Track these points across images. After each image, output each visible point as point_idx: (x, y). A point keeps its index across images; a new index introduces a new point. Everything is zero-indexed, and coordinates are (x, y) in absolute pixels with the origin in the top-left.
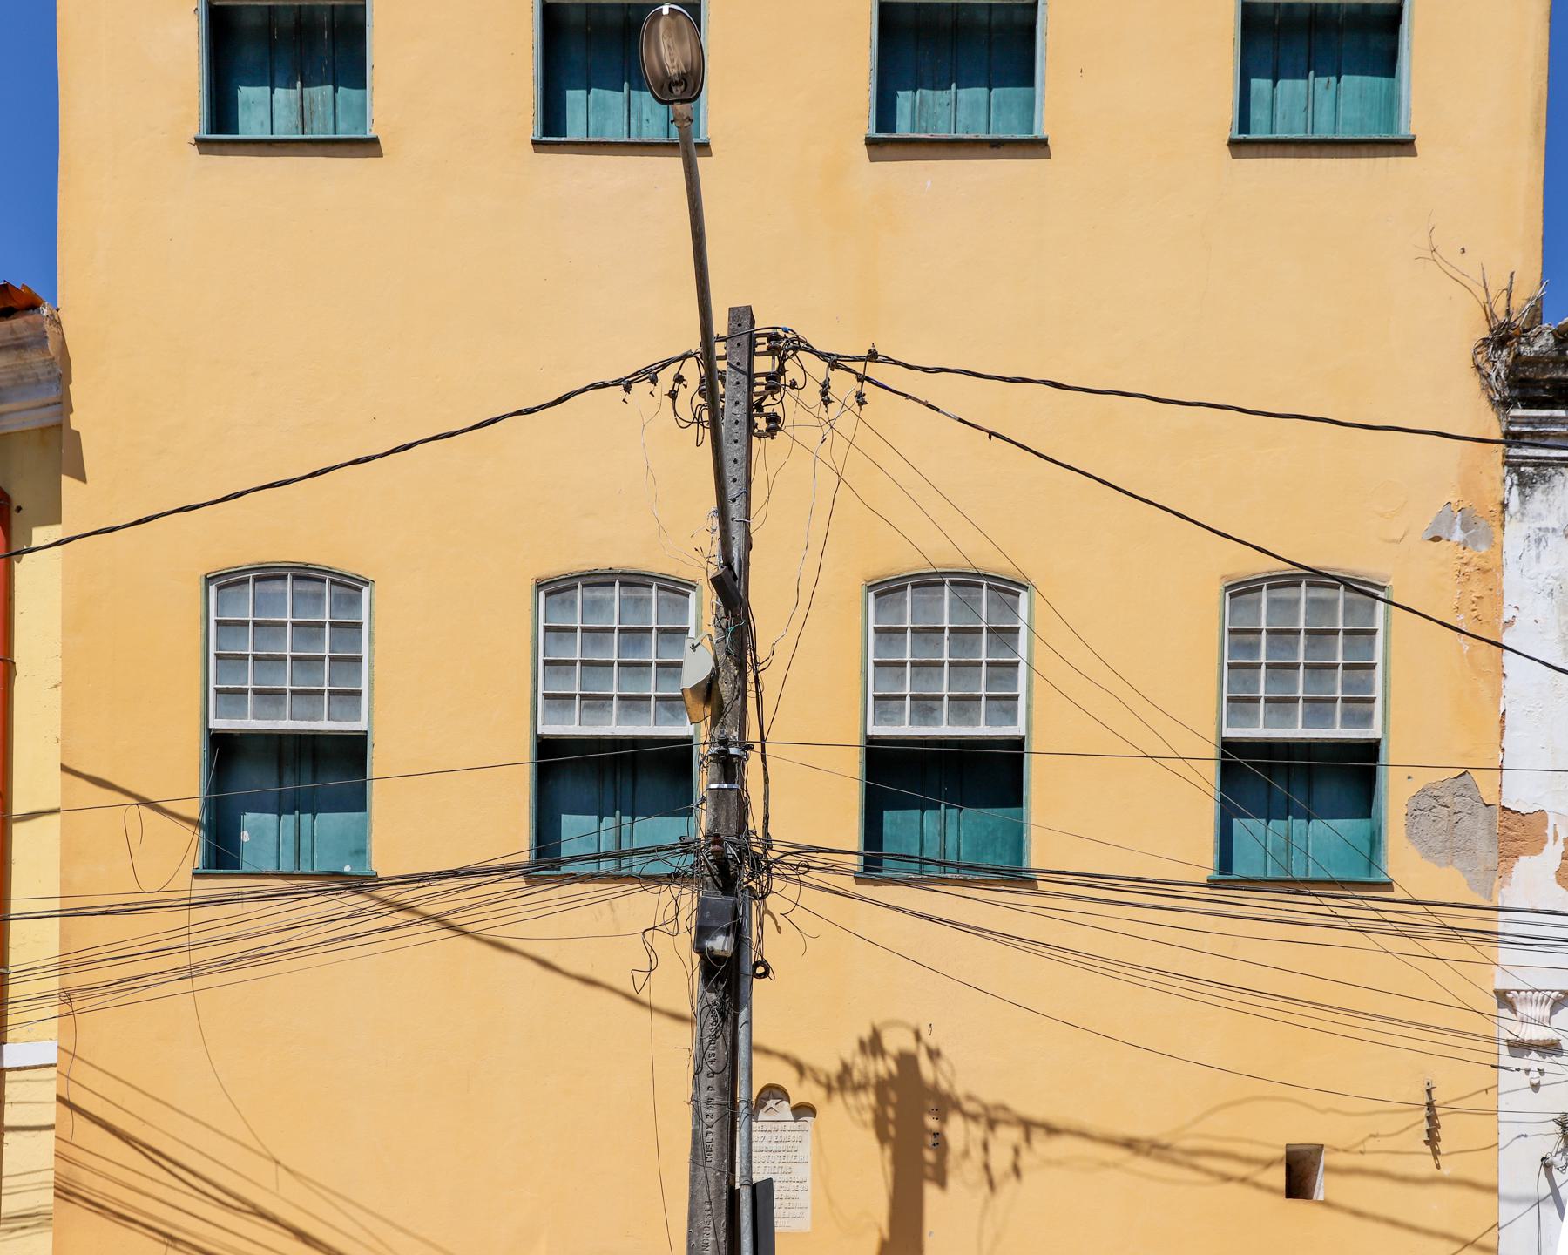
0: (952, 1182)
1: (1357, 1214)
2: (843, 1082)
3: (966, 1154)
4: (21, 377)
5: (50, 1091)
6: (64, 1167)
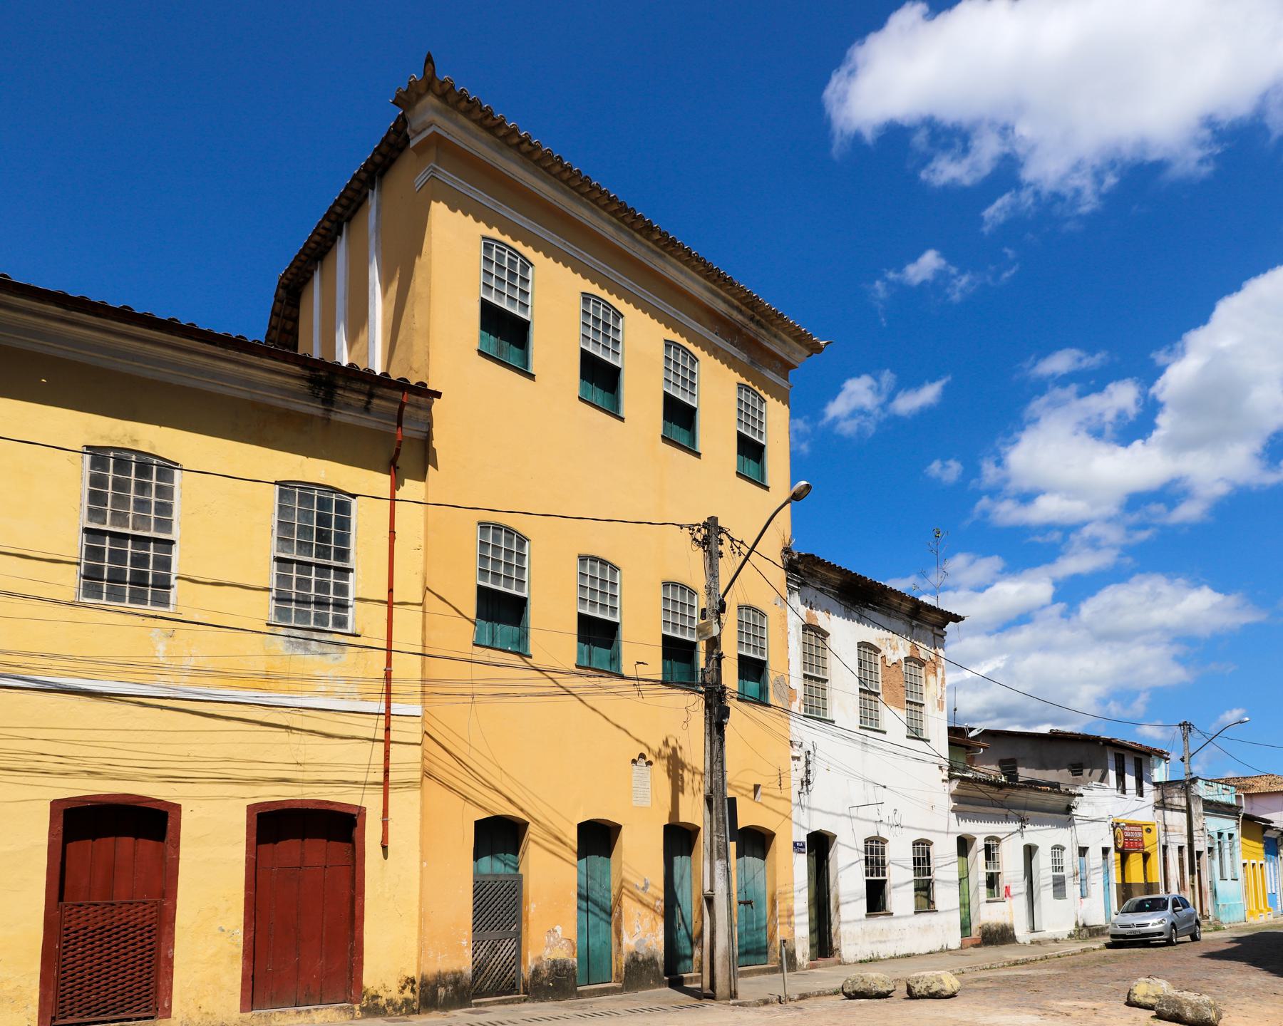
2: (659, 755)
5: (418, 729)
6: (426, 762)
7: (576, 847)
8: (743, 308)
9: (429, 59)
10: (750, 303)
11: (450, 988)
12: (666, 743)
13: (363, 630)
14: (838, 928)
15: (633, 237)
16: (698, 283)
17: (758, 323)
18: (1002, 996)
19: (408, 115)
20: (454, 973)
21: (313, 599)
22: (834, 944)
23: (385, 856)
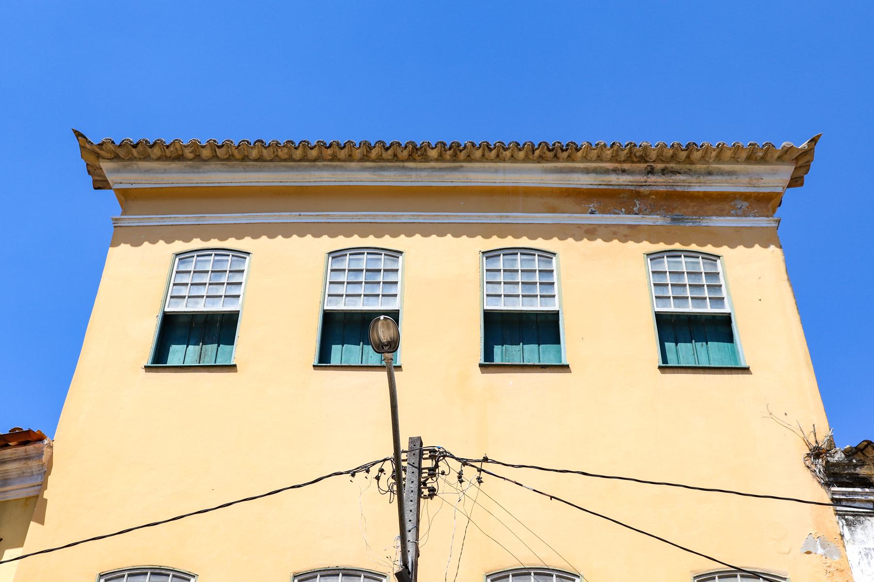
4: (24, 473)
8: (626, 166)
9: (78, 134)
10: (636, 156)
15: (404, 168)
16: (530, 171)
17: (664, 172)
18: (213, 166)
19: (111, 193)
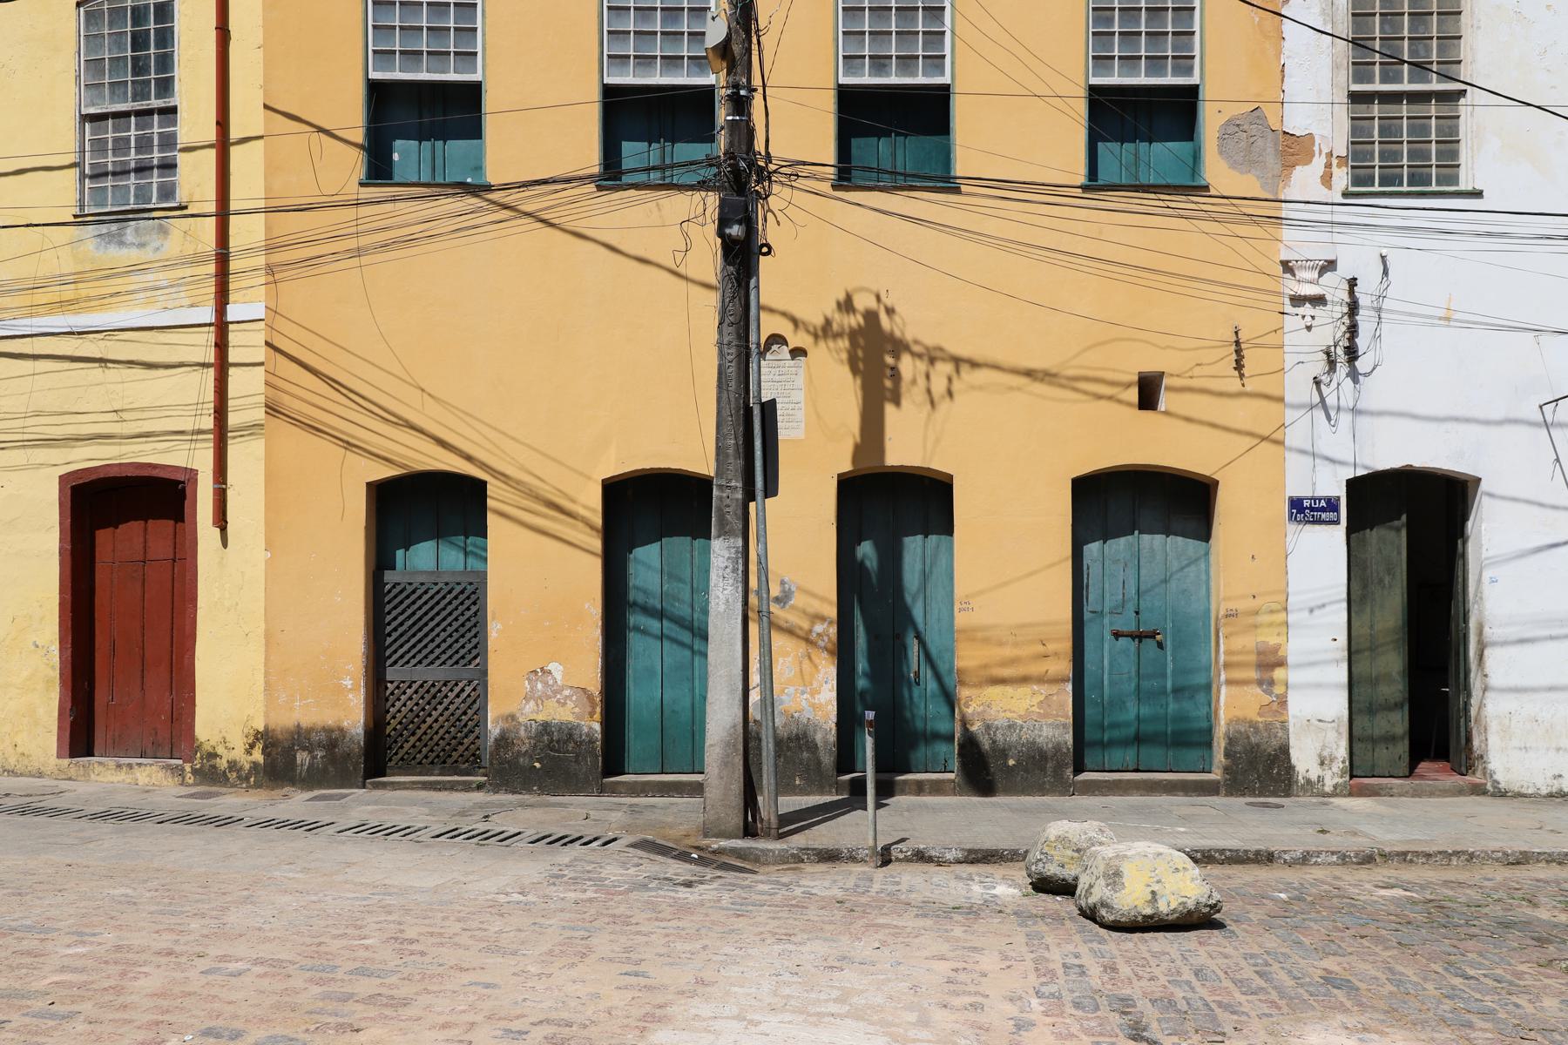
0: (904, 402)
1: (1188, 420)
2: (826, 331)
3: (914, 382)
5: (260, 339)
7: (598, 520)
11: (320, 754)
12: (847, 305)
13: (191, 195)
14: (1481, 706)
20: (328, 730)
21: (155, 162)
22: (1476, 743)
23: (225, 544)
